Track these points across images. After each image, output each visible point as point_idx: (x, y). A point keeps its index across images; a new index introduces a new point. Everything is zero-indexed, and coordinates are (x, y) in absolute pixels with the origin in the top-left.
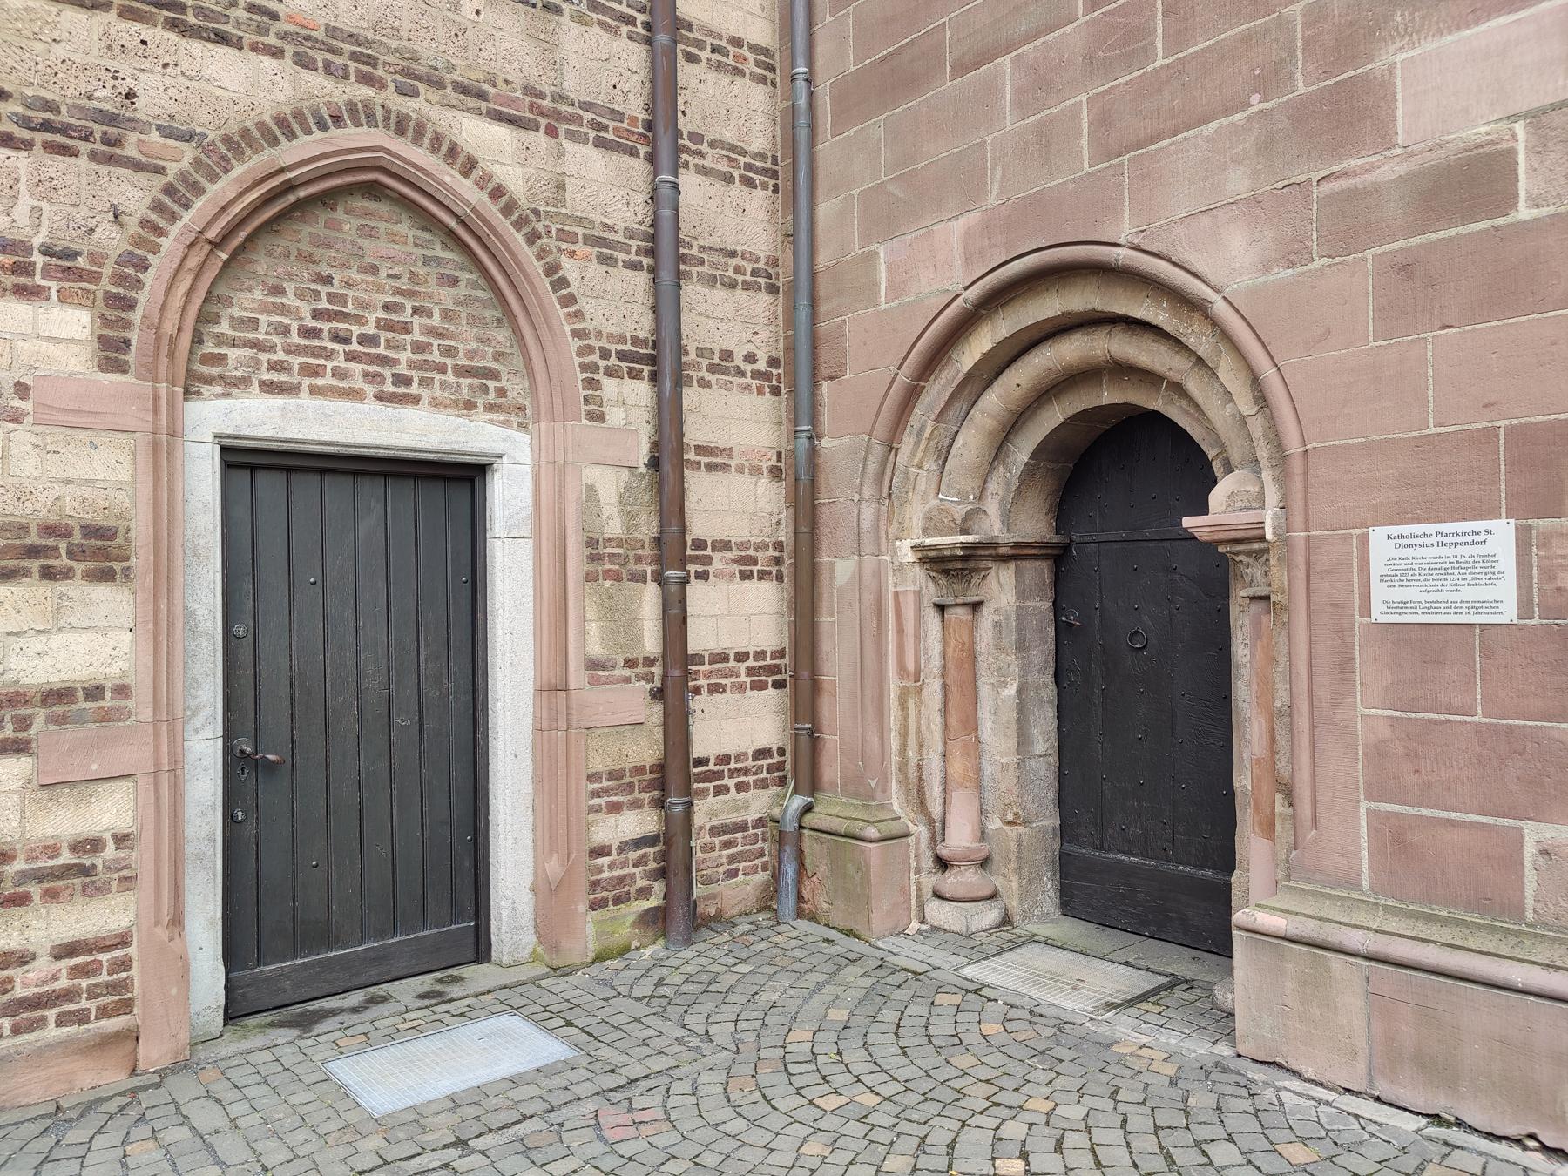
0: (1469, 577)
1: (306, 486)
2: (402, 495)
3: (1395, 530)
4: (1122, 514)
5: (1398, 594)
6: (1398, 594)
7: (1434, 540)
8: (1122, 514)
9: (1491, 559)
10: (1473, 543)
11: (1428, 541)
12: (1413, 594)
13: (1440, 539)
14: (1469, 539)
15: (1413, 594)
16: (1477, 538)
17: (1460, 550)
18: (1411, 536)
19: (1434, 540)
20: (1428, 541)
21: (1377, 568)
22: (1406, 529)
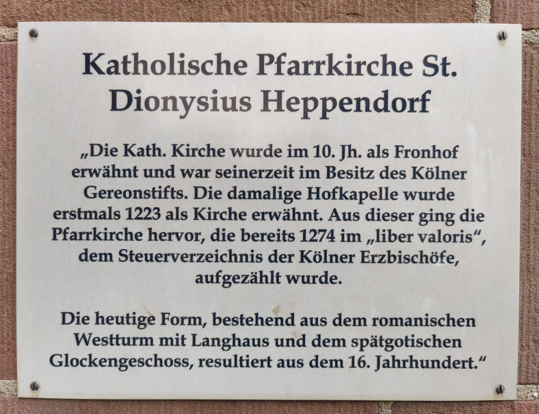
0: (367, 229)
1: (144, 406)
2: (274, 407)
3: (116, 37)
4: (484, 242)
5: (118, 289)
6: (118, 289)
7: (249, 85)
8: (484, 242)
9: (439, 164)
10: (386, 104)
11: (229, 86)
12: (172, 289)
13: (272, 81)
14: (370, 87)
15: (172, 289)
16: (400, 87)
17: (342, 128)
18: (173, 65)
19: (249, 85)
20: (229, 86)
21: (43, 184)
22: (153, 38)
